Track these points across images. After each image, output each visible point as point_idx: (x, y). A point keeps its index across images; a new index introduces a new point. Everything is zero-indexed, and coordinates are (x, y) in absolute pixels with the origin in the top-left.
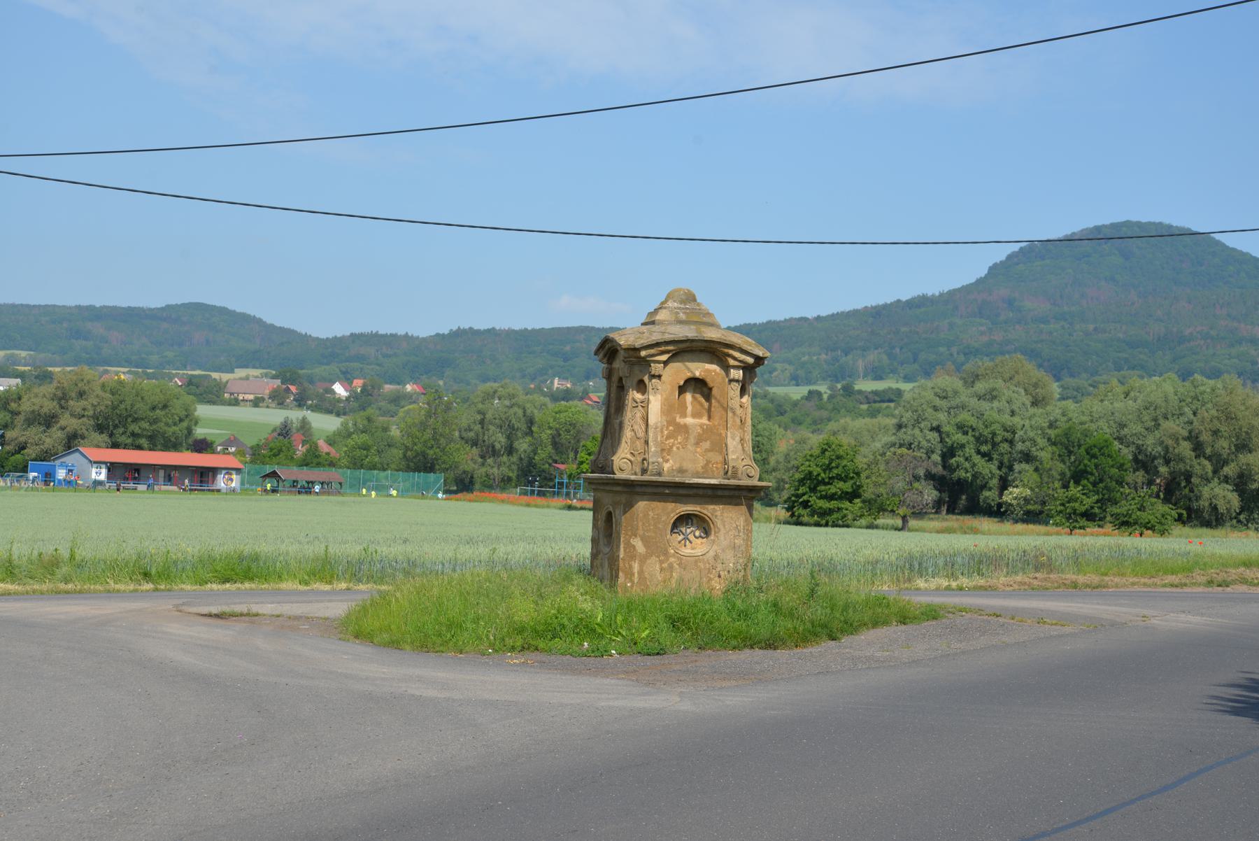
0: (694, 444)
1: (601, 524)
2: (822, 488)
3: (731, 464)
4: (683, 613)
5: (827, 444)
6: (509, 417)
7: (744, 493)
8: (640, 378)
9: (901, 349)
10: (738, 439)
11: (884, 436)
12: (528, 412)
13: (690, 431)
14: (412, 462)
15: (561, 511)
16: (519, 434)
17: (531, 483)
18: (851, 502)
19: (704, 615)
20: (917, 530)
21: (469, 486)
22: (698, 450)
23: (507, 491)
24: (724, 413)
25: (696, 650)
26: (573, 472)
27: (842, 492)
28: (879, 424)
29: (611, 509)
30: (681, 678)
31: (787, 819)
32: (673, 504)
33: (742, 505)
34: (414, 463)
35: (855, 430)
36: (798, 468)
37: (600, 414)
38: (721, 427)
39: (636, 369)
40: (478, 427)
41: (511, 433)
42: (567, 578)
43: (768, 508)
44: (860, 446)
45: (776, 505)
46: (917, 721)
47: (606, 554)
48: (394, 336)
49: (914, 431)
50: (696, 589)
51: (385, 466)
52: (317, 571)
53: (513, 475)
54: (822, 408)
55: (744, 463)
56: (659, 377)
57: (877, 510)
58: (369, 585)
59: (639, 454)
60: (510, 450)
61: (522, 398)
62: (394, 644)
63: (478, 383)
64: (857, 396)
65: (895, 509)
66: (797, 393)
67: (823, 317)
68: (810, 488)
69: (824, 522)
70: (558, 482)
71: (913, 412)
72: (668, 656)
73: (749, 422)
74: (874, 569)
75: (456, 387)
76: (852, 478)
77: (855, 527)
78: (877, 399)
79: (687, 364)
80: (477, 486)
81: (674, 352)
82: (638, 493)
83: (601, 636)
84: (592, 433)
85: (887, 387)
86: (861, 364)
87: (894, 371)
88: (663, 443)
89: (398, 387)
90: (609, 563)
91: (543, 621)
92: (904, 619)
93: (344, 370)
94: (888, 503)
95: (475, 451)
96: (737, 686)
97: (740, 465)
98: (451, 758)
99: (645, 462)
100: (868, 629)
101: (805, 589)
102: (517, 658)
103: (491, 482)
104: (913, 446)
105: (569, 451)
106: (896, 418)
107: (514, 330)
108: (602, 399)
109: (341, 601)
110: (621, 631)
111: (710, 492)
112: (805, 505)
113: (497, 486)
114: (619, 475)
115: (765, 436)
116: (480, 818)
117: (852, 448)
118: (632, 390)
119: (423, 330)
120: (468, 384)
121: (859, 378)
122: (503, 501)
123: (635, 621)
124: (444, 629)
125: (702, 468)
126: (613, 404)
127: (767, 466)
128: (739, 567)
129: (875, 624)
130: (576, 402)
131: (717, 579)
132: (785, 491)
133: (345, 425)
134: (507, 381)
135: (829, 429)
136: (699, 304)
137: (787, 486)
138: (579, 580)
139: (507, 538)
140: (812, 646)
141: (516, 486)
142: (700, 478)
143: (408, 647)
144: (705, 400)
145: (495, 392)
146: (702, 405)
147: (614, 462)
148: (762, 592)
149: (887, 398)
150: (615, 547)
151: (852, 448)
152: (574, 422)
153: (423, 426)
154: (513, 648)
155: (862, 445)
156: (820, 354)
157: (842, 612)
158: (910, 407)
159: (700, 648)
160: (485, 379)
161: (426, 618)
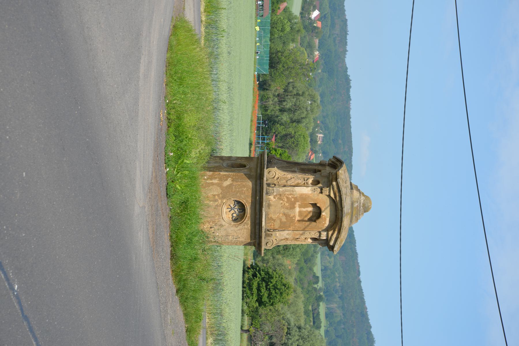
0: (284, 213)
1: (239, 162)
2: (264, 284)
3: (273, 233)
4: (190, 208)
5: (289, 287)
6: (301, 109)
7: (257, 241)
8: (321, 182)
9: (344, 328)
10: (288, 237)
11: (294, 319)
12: (304, 120)
13: (291, 210)
14: (275, 56)
15: (248, 140)
16: (291, 115)
17: (264, 122)
18: (256, 300)
19: (189, 219)
20: (241, 338)
21: (262, 88)
22: (281, 215)
23: (260, 109)
24: (302, 229)
25: (170, 215)
26: (270, 146)
27: (262, 296)
28: (301, 316)
29: (247, 167)
30: (153, 207)
31: (73, 267)
32: (250, 201)
33: (251, 240)
34: (275, 57)
35: (297, 302)
36: (275, 271)
37: (303, 160)
38: (294, 227)
39: (325, 180)
40: (295, 92)
41: (292, 110)
42: (208, 143)
43: (252, 254)
44: (288, 306)
45: (254, 259)
46: (130, 339)
47: (222, 165)
48: (346, 44)
49: (297, 336)
50: (203, 214)
51: (272, 41)
52: (211, 4)
53: (269, 112)
54: (309, 284)
55: (274, 240)
56: (321, 193)
57: (252, 315)
58: (204, 33)
59: (278, 182)
60: (282, 110)
61: (312, 116)
62: (170, 48)
63: (320, 92)
64: (316, 304)
65: (253, 326)
66: (317, 270)
67: (361, 284)
68: (264, 277)
69: (245, 285)
70: (265, 138)
71: (308, 335)
72: (166, 200)
73: (297, 243)
74: (218, 314)
75: (317, 79)
76: (270, 301)
77: (243, 304)
78: (315, 315)
79: (329, 208)
80: (262, 93)
81: (335, 200)
82: (256, 181)
83: (176, 163)
84: (292, 156)
85: (321, 320)
86: (334, 306)
87: (331, 324)
88: (284, 195)
89: (317, 47)
90: (217, 166)
91: (184, 130)
92: (189, 331)
93: (327, 16)
94: (256, 322)
95: (281, 91)
96: (149, 238)
97: (273, 238)
98: (105, 80)
99: (274, 185)
100: (183, 311)
101: (205, 275)
102: (163, 116)
103: (264, 100)
104: (289, 335)
105: (282, 143)
106: (304, 326)
107: (350, 111)
108: (312, 161)
109: (194, 18)
110: (180, 173)
111: (257, 221)
112: (254, 275)
113: (262, 104)
114: (266, 171)
115: (293, 252)
116: (70, 96)
117: (287, 301)
118: (313, 178)
119: (350, 60)
120: (319, 86)
121: (327, 305)
122: (254, 107)
123: (185, 181)
124: (179, 75)
125: (271, 217)
126: (306, 167)
127: (275, 254)
128: (216, 239)
129: (186, 315)
130: (310, 147)
131: (209, 226)
132: (262, 264)
133: (296, 17)
134: (321, 108)
135: (297, 288)
136: (363, 214)
137: (265, 265)
138: (208, 150)
139: (232, 110)
140: (173, 280)
141: (262, 114)
142: (265, 216)
143: (168, 55)
144: (309, 218)
145: (315, 101)
146: (306, 216)
147: (273, 168)
148: (203, 251)
149: (316, 321)
150: (226, 169)
151: (287, 301)
152: (299, 146)
153: (295, 62)
154: (169, 114)
155: (289, 307)
156: (339, 283)
157: (192, 296)
158: (311, 334)
159: (171, 217)
160: (322, 96)
161: (185, 65)
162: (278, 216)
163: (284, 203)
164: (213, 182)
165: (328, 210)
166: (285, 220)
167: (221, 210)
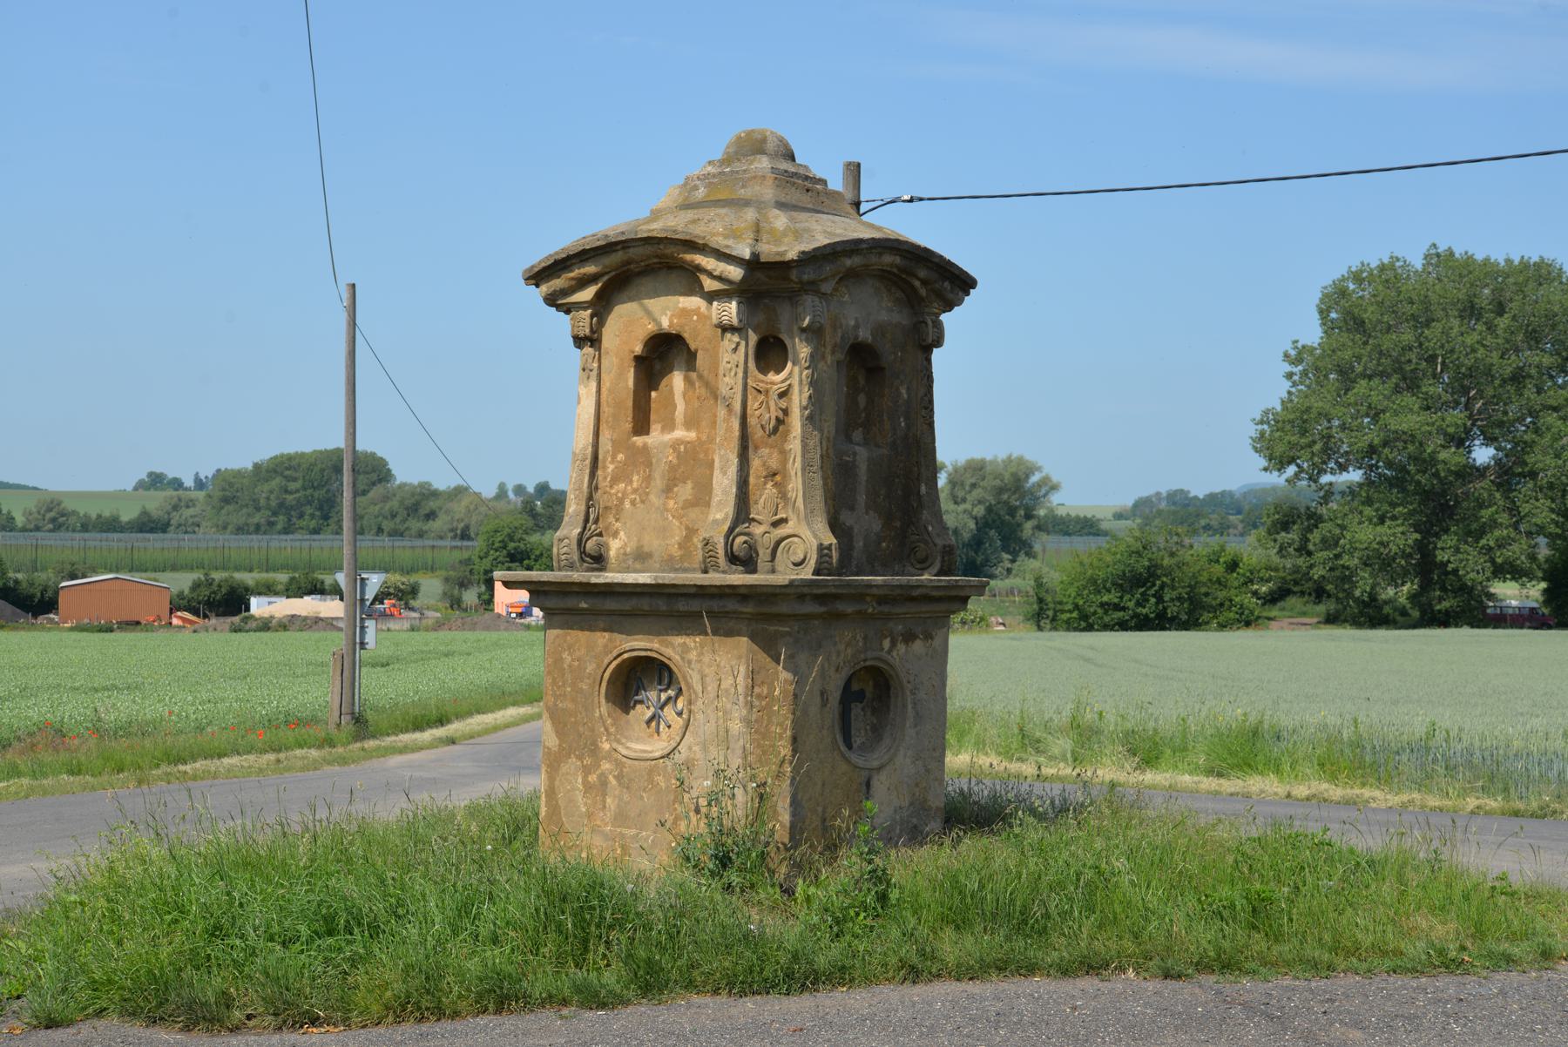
0: (663, 491)
13: (654, 461)
22: (671, 503)
32: (606, 635)
111: (662, 605)
162: (674, 517)
163: (632, 493)
164: (546, 791)
165: (655, 304)
166: (689, 485)
167: (636, 762)
